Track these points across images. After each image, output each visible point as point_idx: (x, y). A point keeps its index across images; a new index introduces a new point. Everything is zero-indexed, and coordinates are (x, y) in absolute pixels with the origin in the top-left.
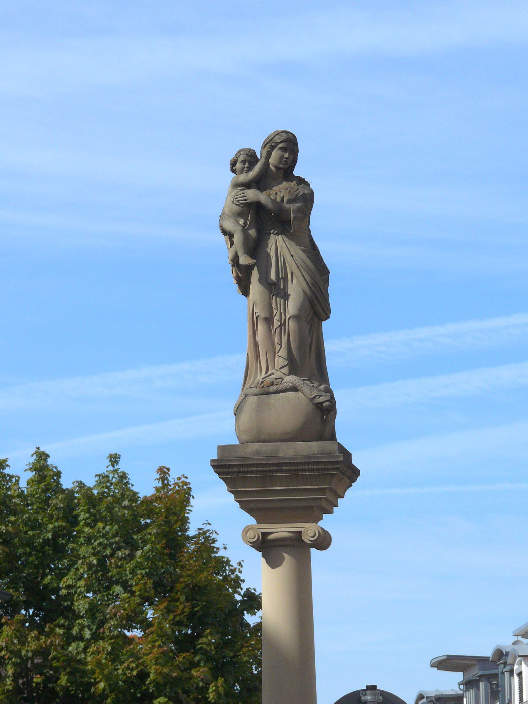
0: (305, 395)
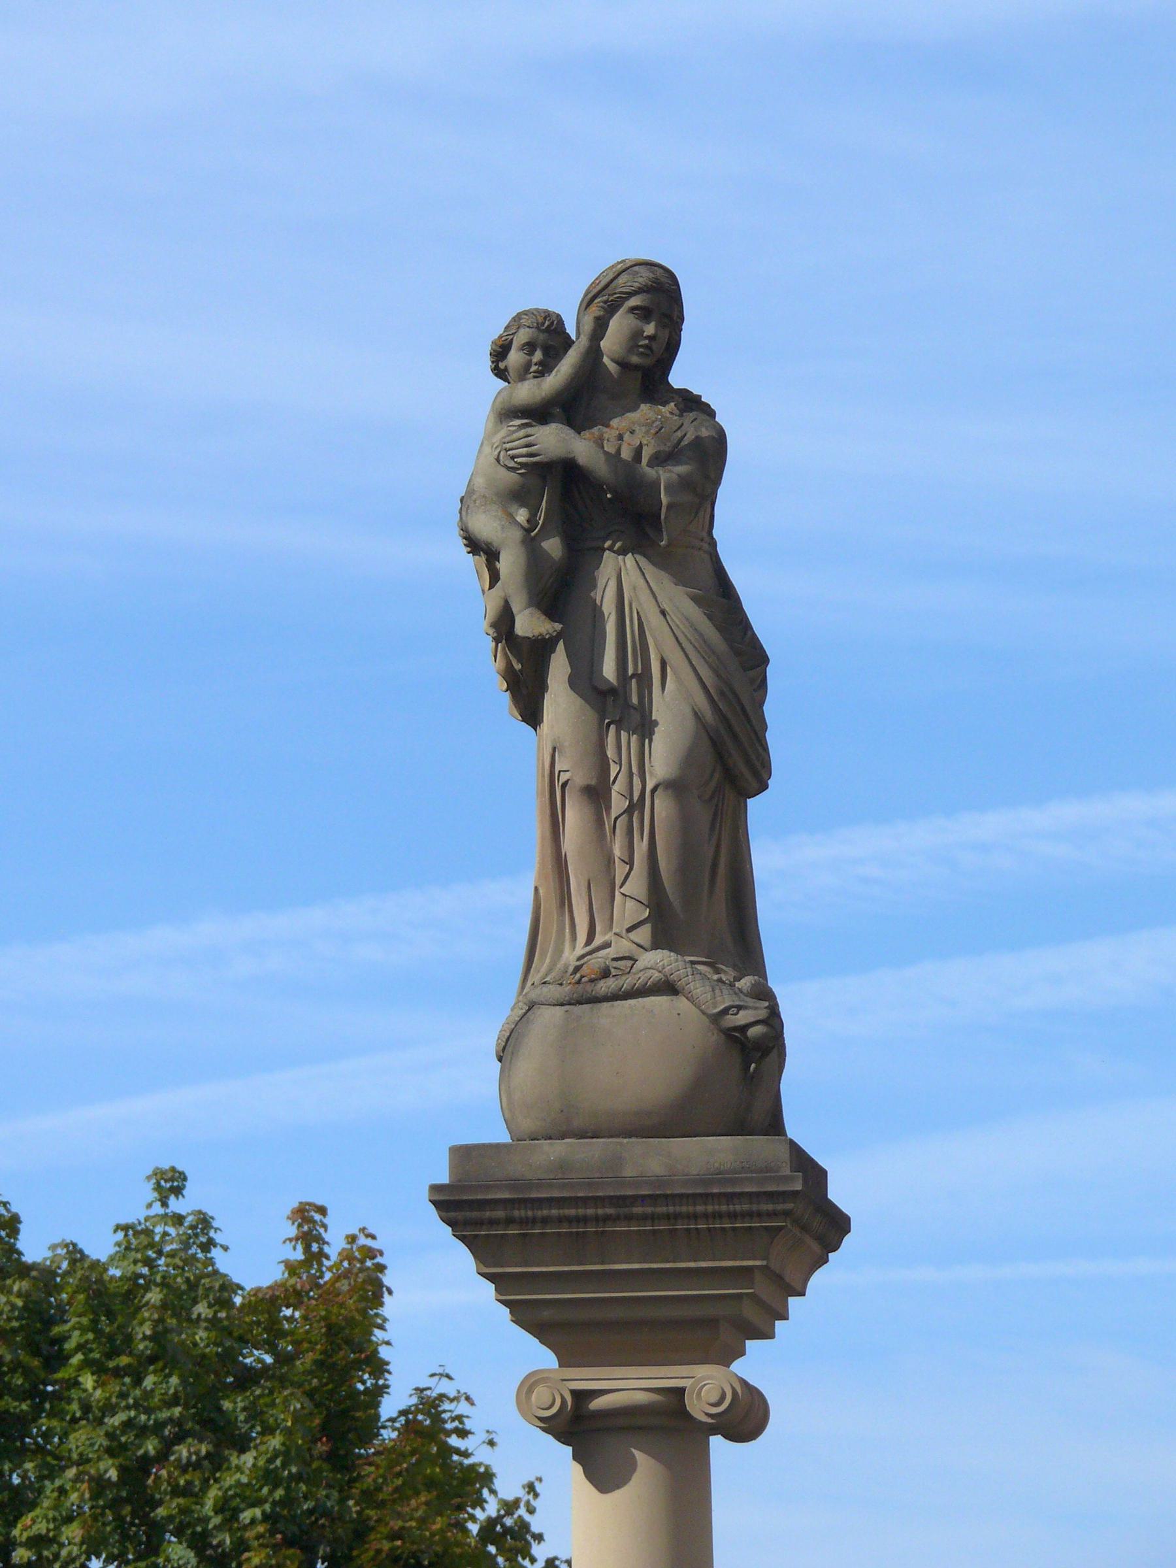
0: (699, 1007)
